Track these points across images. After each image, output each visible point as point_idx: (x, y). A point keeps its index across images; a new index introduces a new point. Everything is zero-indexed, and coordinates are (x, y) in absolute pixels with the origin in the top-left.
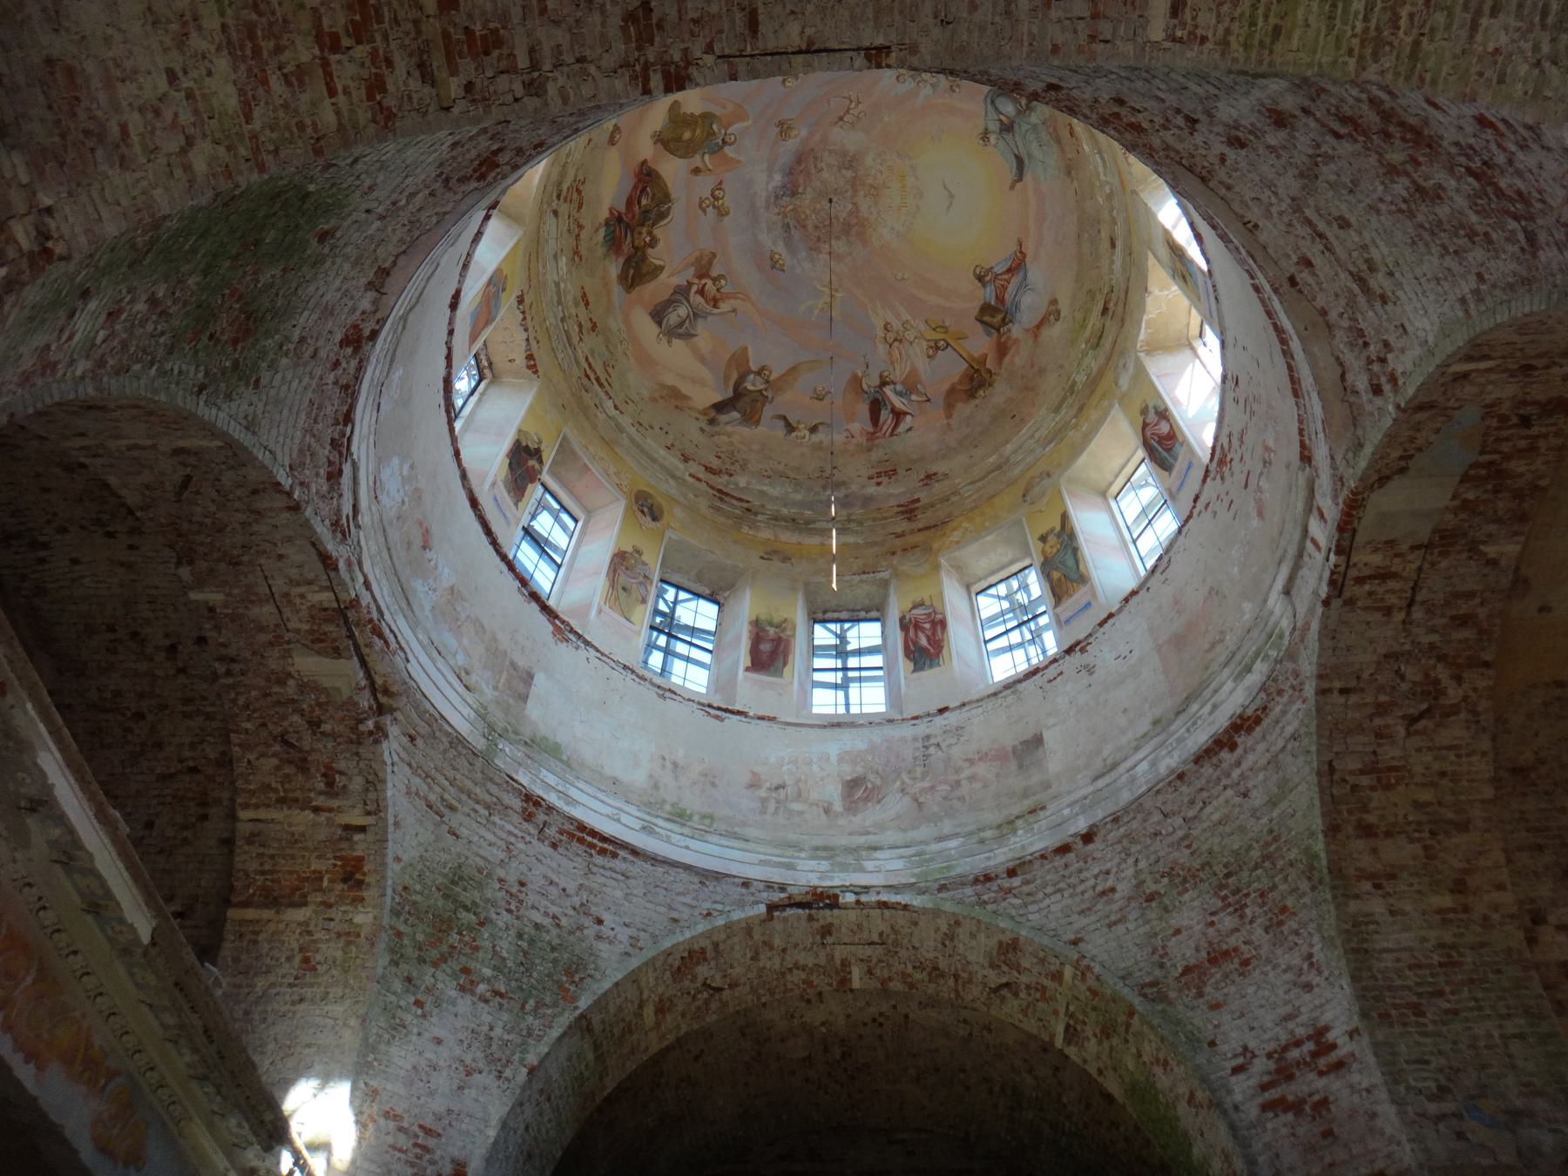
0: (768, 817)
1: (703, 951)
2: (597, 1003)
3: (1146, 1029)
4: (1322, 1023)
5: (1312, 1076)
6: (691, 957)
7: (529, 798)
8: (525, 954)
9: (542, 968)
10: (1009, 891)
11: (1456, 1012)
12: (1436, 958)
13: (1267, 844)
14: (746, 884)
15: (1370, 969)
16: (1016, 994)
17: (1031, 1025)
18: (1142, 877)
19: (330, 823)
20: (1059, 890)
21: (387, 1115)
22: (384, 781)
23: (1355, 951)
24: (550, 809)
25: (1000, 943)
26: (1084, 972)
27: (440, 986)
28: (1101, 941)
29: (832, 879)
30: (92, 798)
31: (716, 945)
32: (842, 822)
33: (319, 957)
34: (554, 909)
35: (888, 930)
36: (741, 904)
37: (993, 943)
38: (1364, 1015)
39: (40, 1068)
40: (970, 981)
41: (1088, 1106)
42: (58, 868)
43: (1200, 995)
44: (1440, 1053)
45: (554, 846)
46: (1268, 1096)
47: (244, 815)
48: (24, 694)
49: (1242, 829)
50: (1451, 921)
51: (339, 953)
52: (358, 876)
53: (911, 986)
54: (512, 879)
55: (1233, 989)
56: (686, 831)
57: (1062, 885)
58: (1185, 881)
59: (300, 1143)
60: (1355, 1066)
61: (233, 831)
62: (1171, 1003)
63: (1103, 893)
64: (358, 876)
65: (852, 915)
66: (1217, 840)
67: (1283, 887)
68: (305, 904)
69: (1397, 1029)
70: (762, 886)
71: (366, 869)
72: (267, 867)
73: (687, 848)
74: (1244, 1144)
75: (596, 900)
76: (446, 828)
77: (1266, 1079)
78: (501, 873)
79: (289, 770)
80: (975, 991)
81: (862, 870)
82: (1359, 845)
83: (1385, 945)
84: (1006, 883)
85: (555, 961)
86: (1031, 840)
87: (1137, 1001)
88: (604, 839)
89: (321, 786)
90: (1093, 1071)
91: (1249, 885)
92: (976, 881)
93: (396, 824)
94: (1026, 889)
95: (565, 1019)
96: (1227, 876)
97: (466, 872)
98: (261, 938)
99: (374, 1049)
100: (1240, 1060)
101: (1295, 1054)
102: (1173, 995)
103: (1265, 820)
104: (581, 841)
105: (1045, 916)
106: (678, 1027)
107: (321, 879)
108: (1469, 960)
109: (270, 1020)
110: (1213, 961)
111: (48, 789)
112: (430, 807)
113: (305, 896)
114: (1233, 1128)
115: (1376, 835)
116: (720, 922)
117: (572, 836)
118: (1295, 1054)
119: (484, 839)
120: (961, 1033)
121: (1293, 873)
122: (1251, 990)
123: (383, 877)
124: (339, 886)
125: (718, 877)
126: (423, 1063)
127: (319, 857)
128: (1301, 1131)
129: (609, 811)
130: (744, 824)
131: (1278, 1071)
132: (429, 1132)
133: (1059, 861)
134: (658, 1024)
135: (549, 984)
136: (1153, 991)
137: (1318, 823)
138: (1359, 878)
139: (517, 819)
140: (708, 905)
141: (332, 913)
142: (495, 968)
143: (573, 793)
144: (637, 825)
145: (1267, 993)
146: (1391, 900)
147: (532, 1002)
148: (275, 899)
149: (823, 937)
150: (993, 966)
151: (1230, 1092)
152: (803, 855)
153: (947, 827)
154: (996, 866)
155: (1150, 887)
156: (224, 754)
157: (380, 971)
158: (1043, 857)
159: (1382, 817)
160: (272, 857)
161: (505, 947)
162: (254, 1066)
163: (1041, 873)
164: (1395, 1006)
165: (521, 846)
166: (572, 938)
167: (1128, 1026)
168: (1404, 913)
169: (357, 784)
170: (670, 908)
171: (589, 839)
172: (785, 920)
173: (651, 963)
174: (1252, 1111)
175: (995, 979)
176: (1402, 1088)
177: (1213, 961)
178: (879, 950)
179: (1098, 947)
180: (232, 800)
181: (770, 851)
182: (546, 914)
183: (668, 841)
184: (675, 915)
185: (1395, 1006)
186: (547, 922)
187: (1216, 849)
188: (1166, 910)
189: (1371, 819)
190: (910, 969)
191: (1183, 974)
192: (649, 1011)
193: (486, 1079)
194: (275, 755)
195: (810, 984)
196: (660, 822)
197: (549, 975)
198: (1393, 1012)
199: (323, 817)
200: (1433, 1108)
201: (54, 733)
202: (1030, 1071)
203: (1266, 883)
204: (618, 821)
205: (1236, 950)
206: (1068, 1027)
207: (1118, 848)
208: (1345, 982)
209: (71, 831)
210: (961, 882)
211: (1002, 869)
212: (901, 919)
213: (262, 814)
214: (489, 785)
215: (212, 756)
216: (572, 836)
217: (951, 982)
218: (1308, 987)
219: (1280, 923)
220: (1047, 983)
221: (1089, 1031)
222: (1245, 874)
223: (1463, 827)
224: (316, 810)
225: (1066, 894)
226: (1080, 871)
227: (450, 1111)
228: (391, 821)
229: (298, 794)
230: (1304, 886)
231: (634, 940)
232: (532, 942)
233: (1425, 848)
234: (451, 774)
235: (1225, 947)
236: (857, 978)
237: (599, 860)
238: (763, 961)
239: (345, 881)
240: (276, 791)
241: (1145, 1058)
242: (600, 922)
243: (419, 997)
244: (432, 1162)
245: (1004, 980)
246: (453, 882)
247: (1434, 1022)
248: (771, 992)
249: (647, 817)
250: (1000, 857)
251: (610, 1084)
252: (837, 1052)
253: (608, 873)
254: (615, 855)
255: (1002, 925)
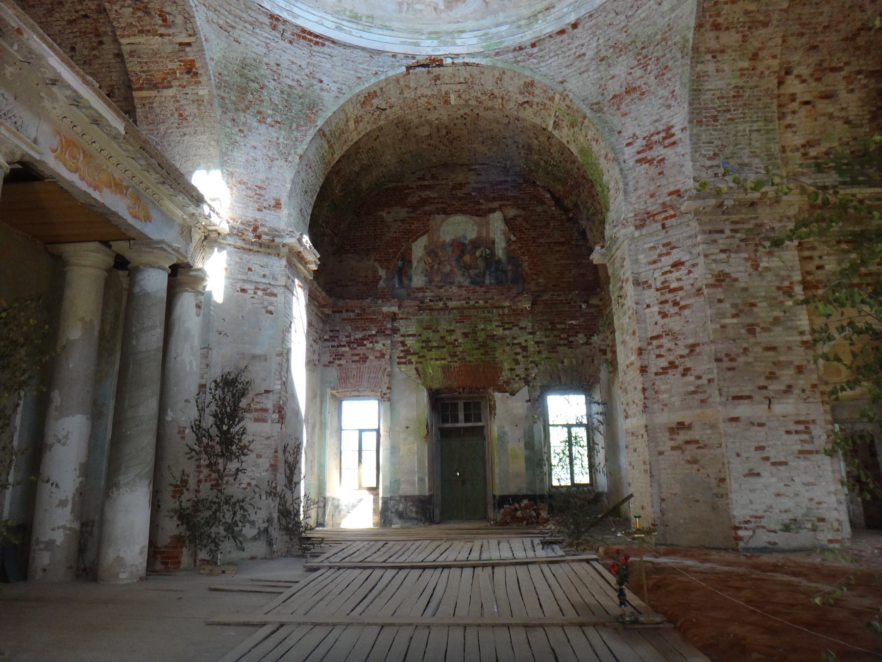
0: (403, 14)
1: (375, 92)
2: (326, 122)
3: (591, 125)
4: (671, 124)
5: (661, 148)
6: (369, 96)
7: (272, 16)
8: (287, 101)
9: (296, 107)
10: (531, 55)
11: (732, 120)
12: (732, 93)
13: (666, 32)
14: (394, 56)
15: (699, 99)
16: (531, 106)
17: (537, 121)
18: (600, 48)
19: (171, 43)
20: (557, 55)
21: (240, 182)
22: (193, 17)
23: (694, 90)
24: (285, 21)
25: (525, 83)
26: (564, 97)
27: (249, 121)
28: (575, 81)
29: (439, 50)
30: (78, 74)
31: (381, 89)
32: (444, 15)
33: (186, 113)
34: (297, 77)
35: (468, 76)
36: (393, 67)
37: (522, 82)
38: (690, 122)
39: (100, 192)
40: (509, 100)
41: (562, 154)
42: (74, 108)
43: (619, 109)
44: (720, 138)
45: (291, 42)
46: (642, 155)
47: (123, 41)
48: (30, 32)
49: (655, 23)
50: (745, 75)
51: (196, 110)
52: (194, 70)
53: (480, 102)
54: (272, 63)
55: (634, 106)
56: (360, 27)
57: (559, 52)
58: (621, 50)
59: (209, 202)
60: (680, 144)
61: (120, 50)
62: (604, 113)
63: (579, 56)
64: (194, 70)
65: (450, 70)
66: (641, 29)
67: (669, 56)
68: (171, 87)
69: (704, 128)
70: (402, 56)
71: (197, 66)
72: (145, 69)
73: (361, 37)
74: (625, 177)
75: (318, 70)
76: (232, 39)
77: (641, 148)
78: (266, 60)
79: (140, 14)
80: (512, 105)
81: (455, 44)
82: (712, 35)
83: (710, 87)
84: (530, 51)
85: (302, 103)
86: (545, 27)
87: (588, 112)
88: (317, 36)
89: (160, 22)
90: (565, 142)
91: (652, 53)
92: (515, 50)
93: (206, 40)
94: (540, 54)
95: (312, 132)
96: (643, 48)
97: (248, 62)
98: (155, 105)
99: (226, 155)
100: (631, 140)
101: (655, 138)
102: (605, 109)
103: (667, 19)
104: (304, 38)
105: (548, 69)
106: (366, 128)
107: (175, 73)
108: (747, 94)
109: (173, 144)
110: (627, 92)
111: (59, 75)
112: (221, 28)
113: (169, 82)
114: (621, 170)
115: (720, 29)
116: (383, 77)
117: (299, 36)
118: (655, 138)
119: (256, 43)
120: (505, 121)
121: (675, 48)
122: (643, 107)
123: (207, 70)
124: (186, 76)
125: (379, 52)
126: (250, 158)
127: (171, 61)
128: (650, 172)
129: (316, 19)
130: (390, 20)
131: (646, 146)
132: (260, 188)
133: (559, 39)
134: (356, 128)
135: (301, 115)
136: (597, 107)
137: (692, 23)
138: (706, 53)
139: (268, 29)
140: (375, 69)
141: (186, 90)
142: (273, 110)
143: (296, 10)
144: (333, 26)
145: (649, 109)
146: (718, 64)
147: (294, 125)
148: (155, 85)
149: (435, 81)
150: (521, 93)
151: (623, 154)
152: (423, 37)
153: (501, 17)
154: (526, 42)
155: (603, 53)
156: (99, 5)
157: (219, 117)
158: (550, 36)
159: (726, 19)
160: (146, 63)
161: (276, 99)
162: (173, 165)
163: (550, 45)
164: (706, 117)
165: (273, 44)
166: (308, 91)
167: (583, 123)
168: (723, 71)
169: (179, 20)
170: (356, 71)
171: (309, 37)
172: (416, 74)
173: (350, 100)
174: (631, 163)
175: (521, 99)
176: (697, 155)
177: (627, 92)
178: (464, 86)
179: (573, 85)
180: (114, 32)
181: (405, 36)
182: (293, 80)
183: (350, 34)
184: (359, 75)
185: (706, 117)
186: (294, 84)
187: (640, 34)
188: (609, 66)
189: (720, 20)
190: (479, 95)
191: (613, 98)
192: (351, 124)
193: (280, 162)
194: (129, 6)
195: (429, 103)
196: (345, 23)
197: (300, 111)
198: (704, 120)
199: (166, 39)
200: (708, 163)
201: (51, 47)
202: (537, 138)
203: (660, 53)
204: (322, 24)
205: (639, 87)
206: (555, 122)
207: (590, 31)
208: (686, 105)
209: (75, 91)
210: (507, 51)
211: (529, 43)
212: (475, 71)
213: (132, 40)
214: (250, 11)
215: (93, 7)
216: (299, 36)
217: (500, 101)
218: (669, 107)
219: (663, 74)
220: (547, 101)
221: (564, 124)
222: (652, 47)
223: (765, 24)
224: (161, 35)
225: (560, 57)
226: (569, 44)
227: (267, 178)
228: (203, 39)
229: (148, 27)
230: (679, 55)
231: (340, 90)
232: (289, 95)
233: (744, 36)
234: (228, 8)
235: (634, 85)
236: (453, 99)
237: (315, 48)
238: (406, 94)
239: (188, 73)
240: (136, 26)
241: (589, 137)
242: (321, 81)
243: (241, 128)
244: (265, 200)
245: (526, 100)
246: (243, 68)
247: (721, 124)
248: (410, 108)
249: (338, 21)
250: (528, 36)
251: (337, 157)
252: (444, 132)
253: (322, 55)
254: (323, 45)
255: (526, 74)
